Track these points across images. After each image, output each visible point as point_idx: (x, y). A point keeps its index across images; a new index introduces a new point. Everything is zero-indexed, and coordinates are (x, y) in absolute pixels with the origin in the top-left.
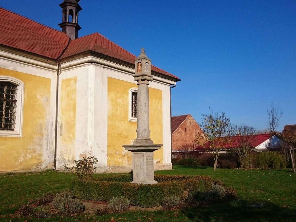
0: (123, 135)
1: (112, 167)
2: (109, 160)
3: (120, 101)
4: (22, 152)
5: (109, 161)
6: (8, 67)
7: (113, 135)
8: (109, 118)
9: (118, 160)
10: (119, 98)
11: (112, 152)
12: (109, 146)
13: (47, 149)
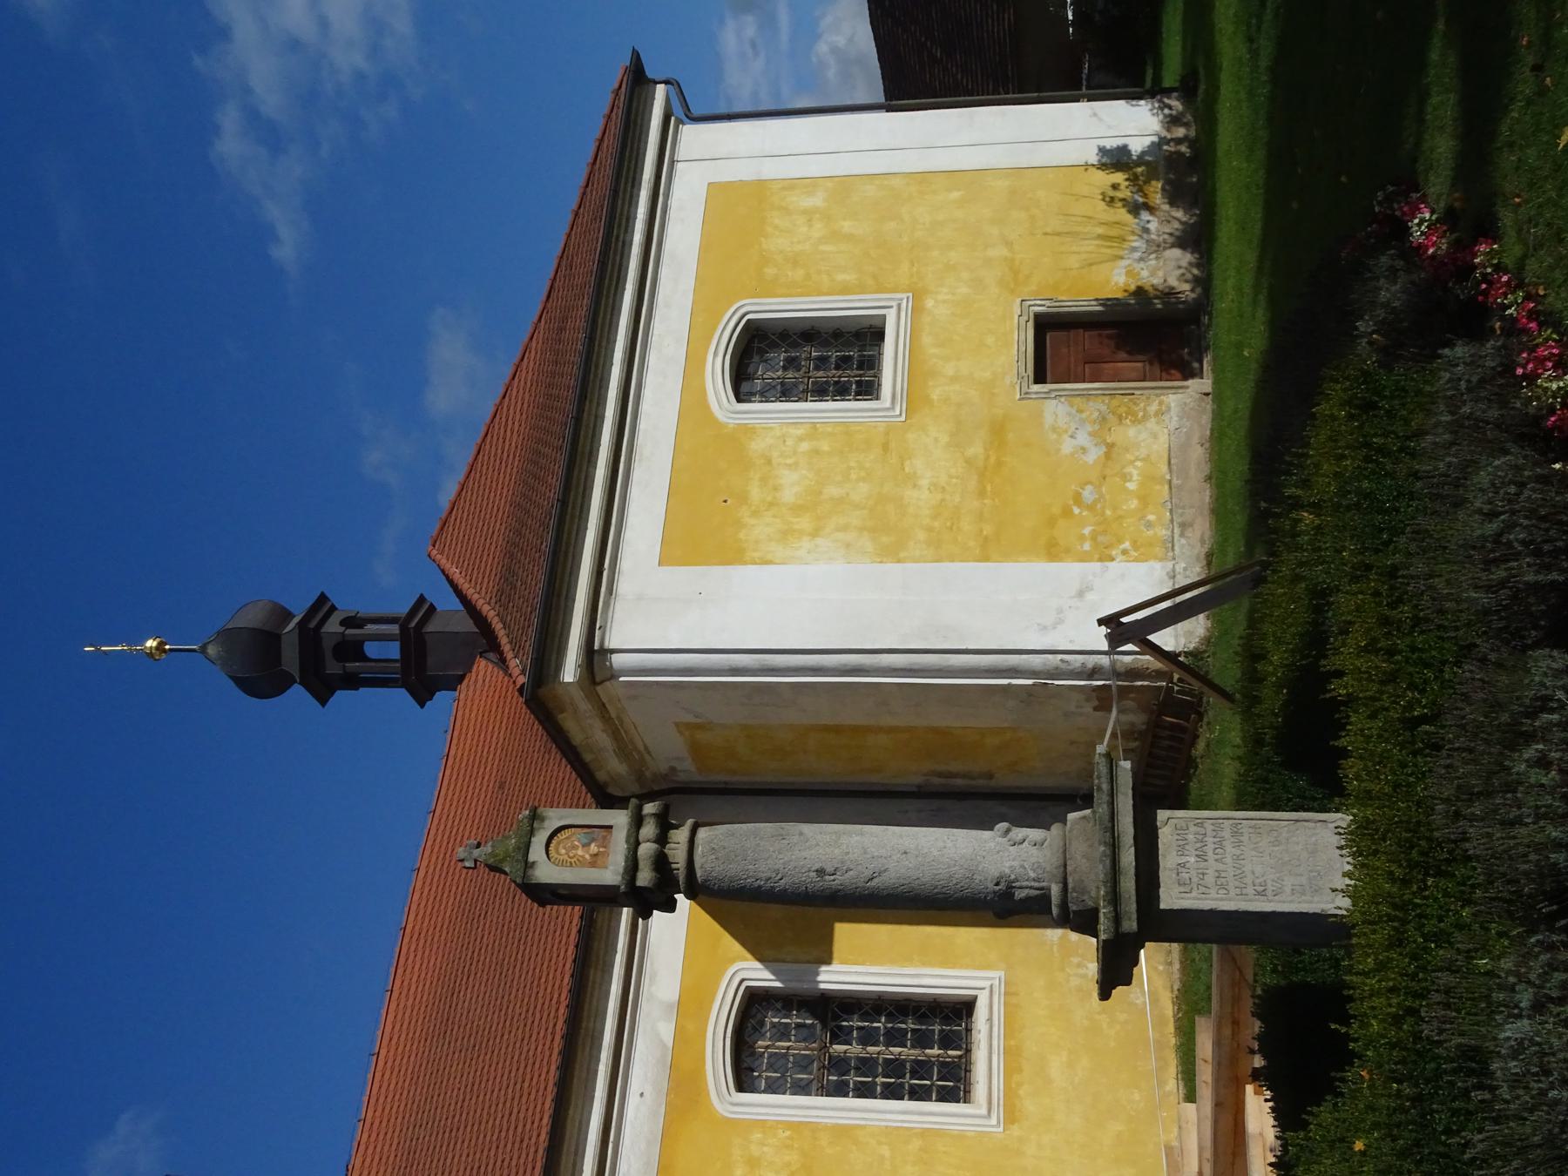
0: (987, 458)
1: (1177, 531)
3: (792, 484)
4: (1081, 971)
6: (665, 1046)
7: (988, 530)
8: (892, 552)
9: (1131, 486)
10: (776, 489)
11: (1087, 531)
12: (1054, 551)
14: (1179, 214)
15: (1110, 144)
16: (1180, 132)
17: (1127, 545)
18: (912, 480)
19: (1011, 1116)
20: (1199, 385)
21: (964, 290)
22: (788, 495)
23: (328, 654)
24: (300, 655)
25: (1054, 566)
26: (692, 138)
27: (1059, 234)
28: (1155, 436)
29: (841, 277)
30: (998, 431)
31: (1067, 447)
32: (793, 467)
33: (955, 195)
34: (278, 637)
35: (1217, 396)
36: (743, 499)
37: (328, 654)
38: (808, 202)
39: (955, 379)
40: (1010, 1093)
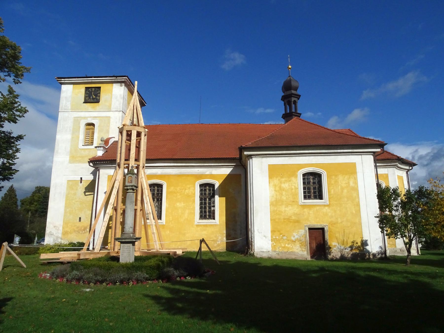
2: (274, 246)
3: (285, 186)
5: (273, 247)
7: (277, 220)
8: (272, 204)
9: (287, 245)
11: (277, 237)
12: (273, 232)
13: (241, 234)
14: (349, 256)
15: (369, 242)
16: (371, 257)
17: (275, 244)
18: (287, 206)
19: (197, 226)
20: (309, 258)
21: (330, 214)
22: (283, 185)
24: (289, 95)
25: (270, 232)
27: (344, 232)
28: (297, 249)
29: (332, 191)
30: (298, 221)
31: (295, 234)
33: (354, 212)
34: (291, 90)
35: (306, 261)
36: (282, 177)
39: (309, 213)
40: (201, 225)
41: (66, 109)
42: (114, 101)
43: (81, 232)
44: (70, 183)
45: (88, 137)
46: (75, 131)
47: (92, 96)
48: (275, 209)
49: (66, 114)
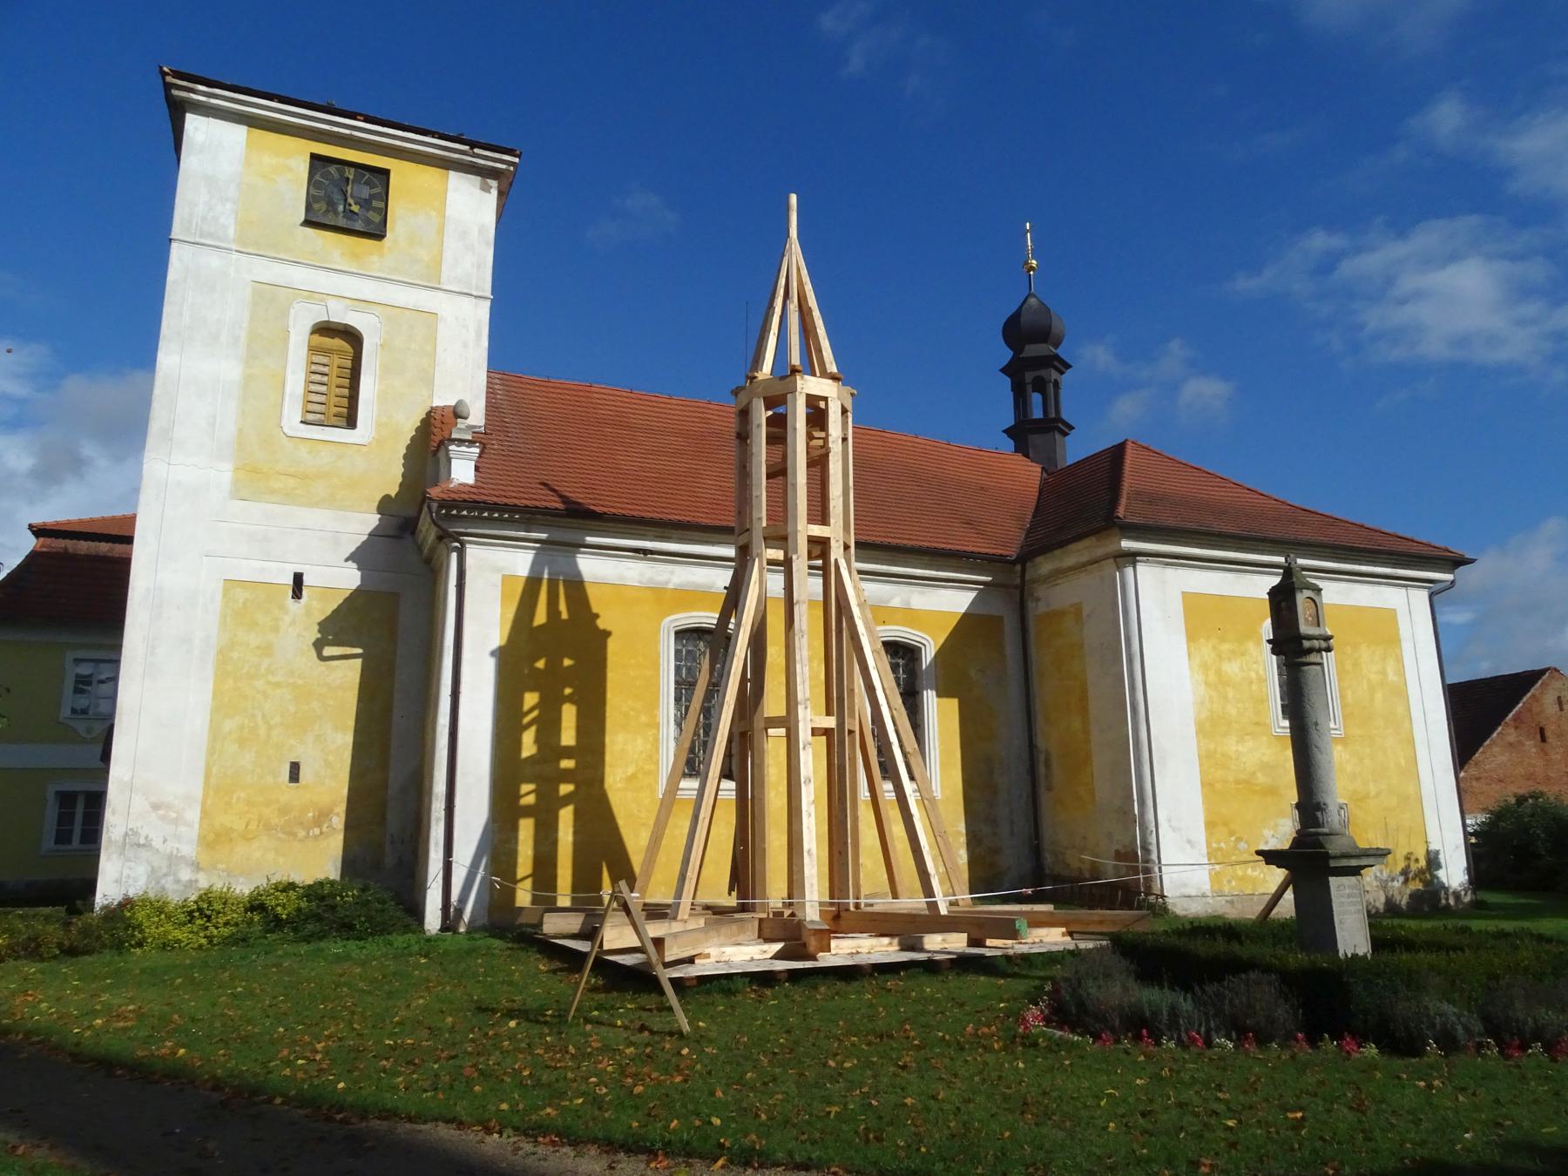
3: (1232, 668)
5: (1215, 878)
7: (1218, 786)
8: (1201, 730)
12: (1210, 825)
13: (1012, 833)
15: (1441, 857)
16: (1452, 902)
18: (1241, 740)
21: (1349, 769)
23: (1037, 373)
24: (1032, 353)
26: (1420, 597)
29: (1349, 693)
31: (1267, 833)
32: (1241, 669)
36: (1222, 640)
37: (1037, 373)
38: (1390, 671)
41: (211, 235)
42: (451, 246)
43: (302, 834)
44: (241, 595)
45: (323, 389)
46: (261, 346)
47: (348, 203)
48: (1212, 746)
49: (213, 261)
